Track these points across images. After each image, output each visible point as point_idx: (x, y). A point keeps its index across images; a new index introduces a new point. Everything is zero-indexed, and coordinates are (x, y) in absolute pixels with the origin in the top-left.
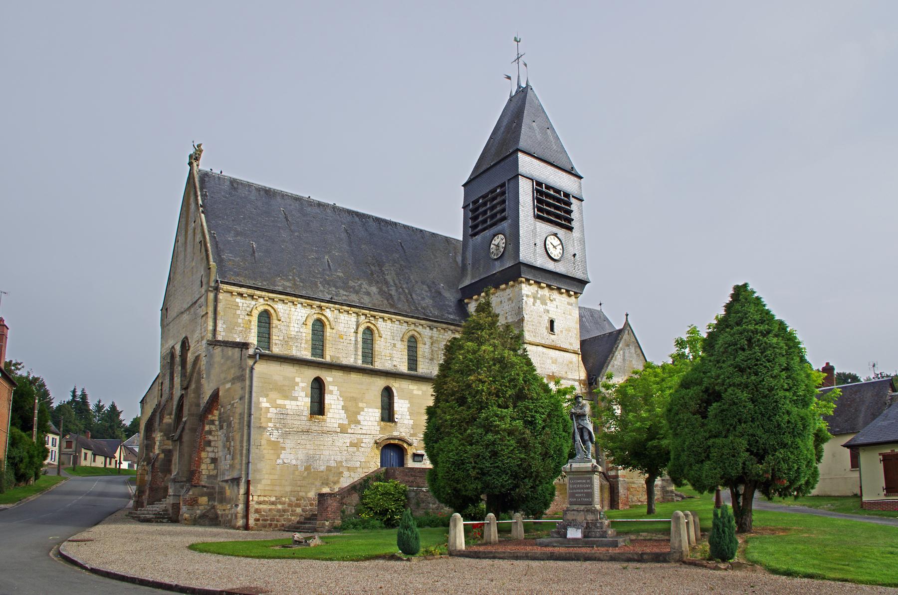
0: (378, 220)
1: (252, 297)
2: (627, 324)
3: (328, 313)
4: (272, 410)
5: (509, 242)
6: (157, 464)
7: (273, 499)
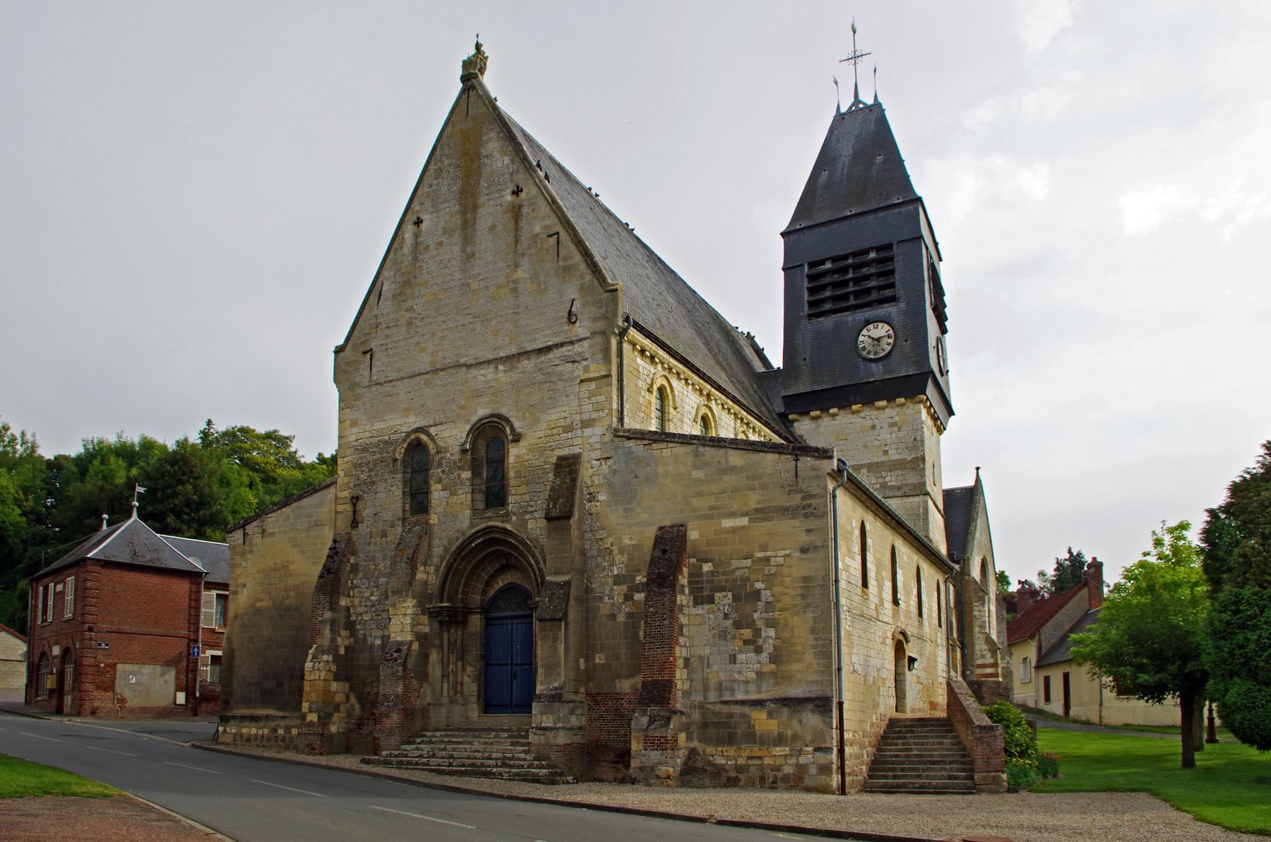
2: (978, 480)
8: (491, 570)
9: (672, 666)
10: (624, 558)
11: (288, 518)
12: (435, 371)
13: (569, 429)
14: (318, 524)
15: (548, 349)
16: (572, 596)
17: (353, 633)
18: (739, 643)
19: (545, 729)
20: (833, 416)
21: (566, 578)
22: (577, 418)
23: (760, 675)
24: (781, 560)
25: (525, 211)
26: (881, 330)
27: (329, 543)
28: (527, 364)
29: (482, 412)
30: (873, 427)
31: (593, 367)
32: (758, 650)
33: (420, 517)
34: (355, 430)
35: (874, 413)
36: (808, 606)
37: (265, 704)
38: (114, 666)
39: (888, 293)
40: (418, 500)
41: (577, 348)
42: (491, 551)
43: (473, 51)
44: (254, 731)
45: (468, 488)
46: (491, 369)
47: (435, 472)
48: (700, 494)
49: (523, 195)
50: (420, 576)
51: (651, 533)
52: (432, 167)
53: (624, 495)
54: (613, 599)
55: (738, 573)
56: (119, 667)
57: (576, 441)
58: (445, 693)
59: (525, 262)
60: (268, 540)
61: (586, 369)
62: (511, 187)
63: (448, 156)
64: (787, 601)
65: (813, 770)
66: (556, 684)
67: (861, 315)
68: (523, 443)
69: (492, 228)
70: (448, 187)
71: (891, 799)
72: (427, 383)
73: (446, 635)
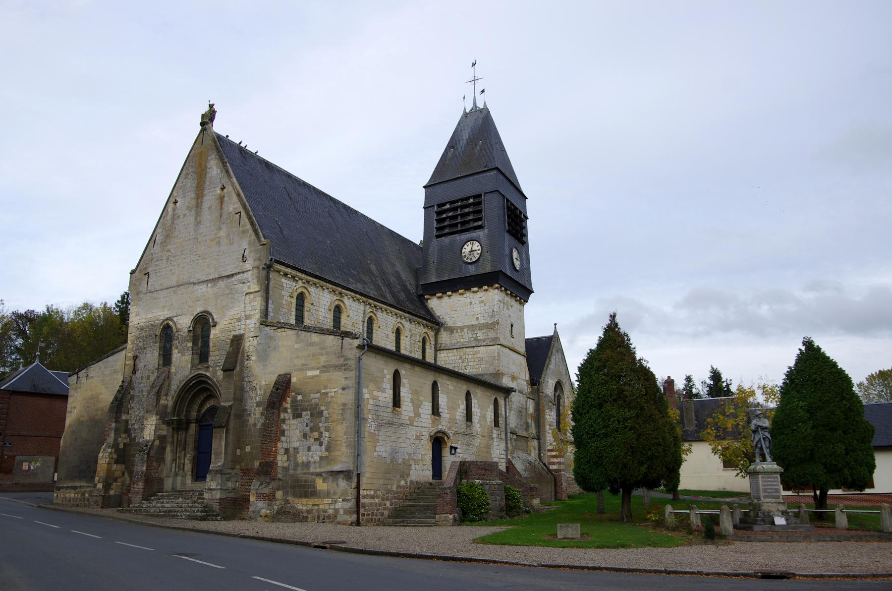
0: (344, 206)
1: (293, 277)
2: (555, 331)
3: (345, 299)
4: (371, 401)
5: (485, 250)
6: (152, 453)
7: (372, 493)
8: (202, 398)
9: (276, 453)
10: (262, 392)
11: (100, 368)
12: (178, 286)
13: (239, 320)
14: (116, 372)
15: (232, 275)
16: (232, 414)
17: (129, 435)
18: (312, 440)
19: (211, 490)
20: (449, 296)
21: (230, 404)
22: (243, 314)
23: (321, 458)
24: (333, 394)
25: (226, 199)
26: (476, 246)
27: (120, 383)
28: (221, 284)
29: (199, 309)
30: (471, 303)
31: (252, 286)
32: (321, 444)
33: (166, 369)
34: (138, 318)
35: (471, 295)
36: (344, 420)
37: (80, 478)
38: (13, 457)
39: (480, 223)
40: (166, 357)
41: (245, 275)
42: (198, 388)
43: (207, 108)
44: (73, 495)
45: (190, 352)
46: (205, 286)
47: (175, 342)
48: (298, 357)
49: (225, 190)
50: (162, 402)
51: (274, 378)
52: (184, 172)
53: (264, 356)
54: (256, 415)
55: (313, 401)
56: (18, 458)
57: (243, 327)
58: (173, 470)
59: (224, 227)
60: (89, 381)
61: (249, 287)
62: (220, 186)
63: (192, 167)
64: (335, 417)
65: (341, 512)
66: (220, 464)
67: (465, 236)
68: (217, 327)
69: (210, 208)
70: (190, 183)
71: (32, 494)
72: (175, 292)
73: (175, 436)
